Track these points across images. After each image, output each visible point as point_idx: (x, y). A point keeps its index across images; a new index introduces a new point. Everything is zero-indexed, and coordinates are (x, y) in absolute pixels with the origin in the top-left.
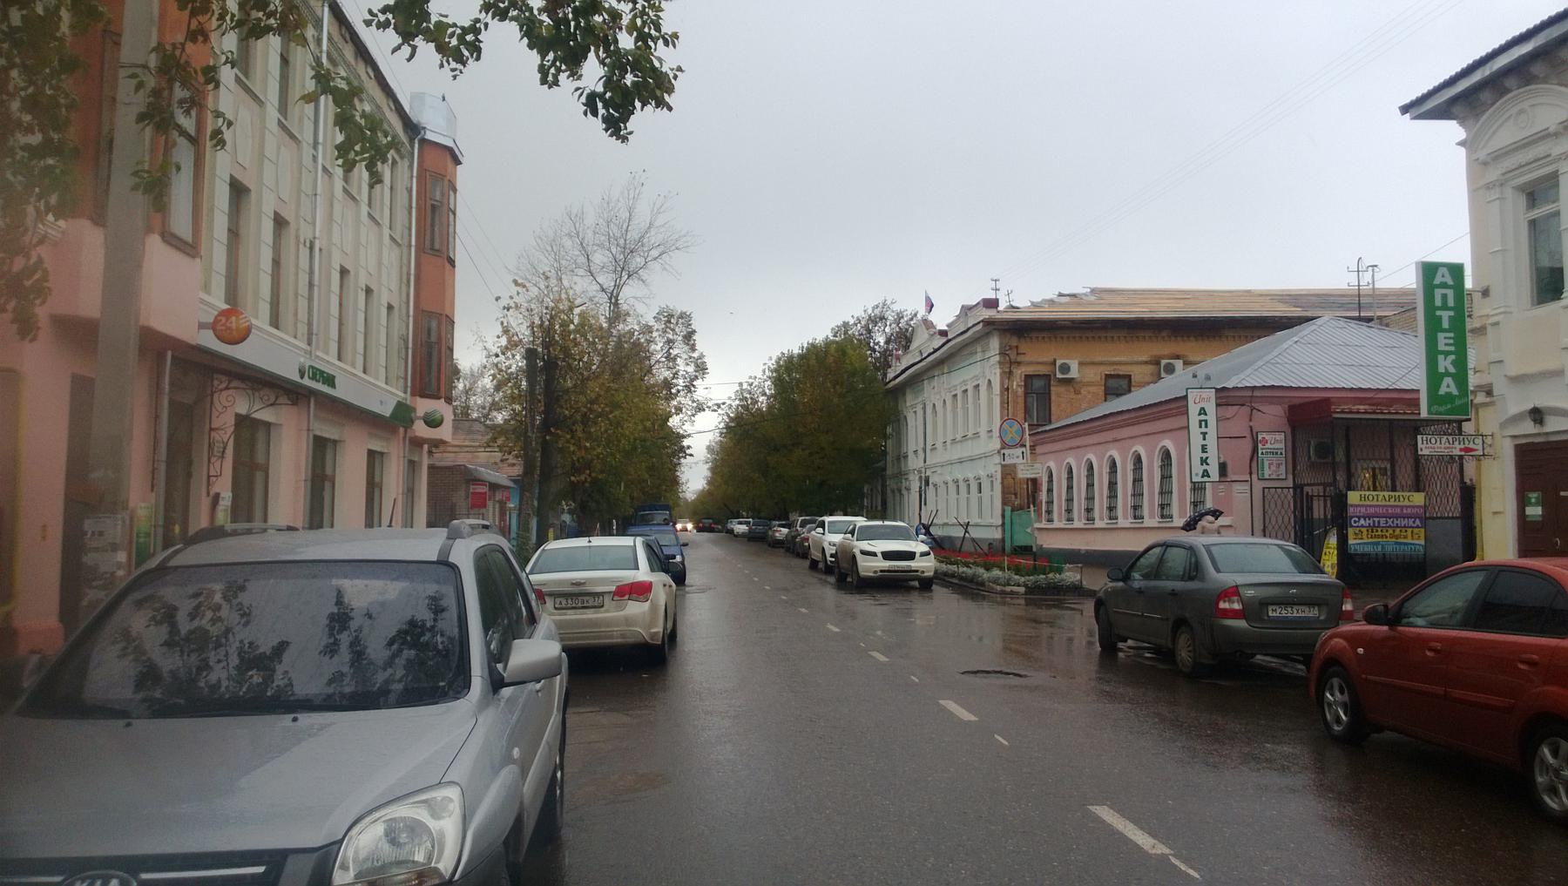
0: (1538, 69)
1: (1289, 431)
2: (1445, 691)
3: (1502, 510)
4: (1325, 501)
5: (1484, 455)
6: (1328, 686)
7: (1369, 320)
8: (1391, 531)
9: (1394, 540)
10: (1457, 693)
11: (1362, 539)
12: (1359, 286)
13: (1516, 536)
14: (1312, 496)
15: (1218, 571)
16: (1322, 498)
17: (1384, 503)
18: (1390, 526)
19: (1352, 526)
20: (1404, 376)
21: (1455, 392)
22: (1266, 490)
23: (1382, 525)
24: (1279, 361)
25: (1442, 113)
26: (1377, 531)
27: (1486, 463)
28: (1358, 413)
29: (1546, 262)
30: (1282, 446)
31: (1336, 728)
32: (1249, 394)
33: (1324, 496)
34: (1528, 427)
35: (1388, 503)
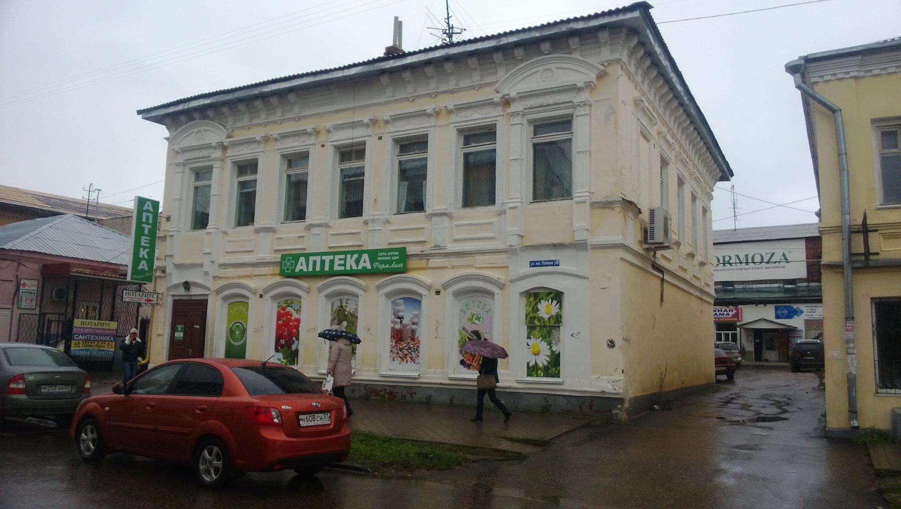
0: (210, 113)
1: (40, 278)
2: (156, 427)
3: (162, 333)
4: (59, 324)
5: (157, 304)
6: (84, 430)
7: (92, 220)
8: (96, 343)
9: (98, 348)
10: (161, 428)
11: (79, 347)
12: (89, 199)
13: (168, 348)
14: (51, 321)
15: (10, 364)
16: (57, 322)
17: (94, 327)
18: (96, 340)
19: (74, 339)
20: (117, 256)
21: (147, 269)
22: (22, 315)
23: (92, 339)
24: (40, 237)
25: (159, 120)
26: (88, 343)
27: (156, 308)
28: (85, 273)
29: (199, 209)
30: (36, 288)
31: (87, 454)
32: (19, 254)
33: (59, 321)
34: (182, 291)
35: (97, 327)
